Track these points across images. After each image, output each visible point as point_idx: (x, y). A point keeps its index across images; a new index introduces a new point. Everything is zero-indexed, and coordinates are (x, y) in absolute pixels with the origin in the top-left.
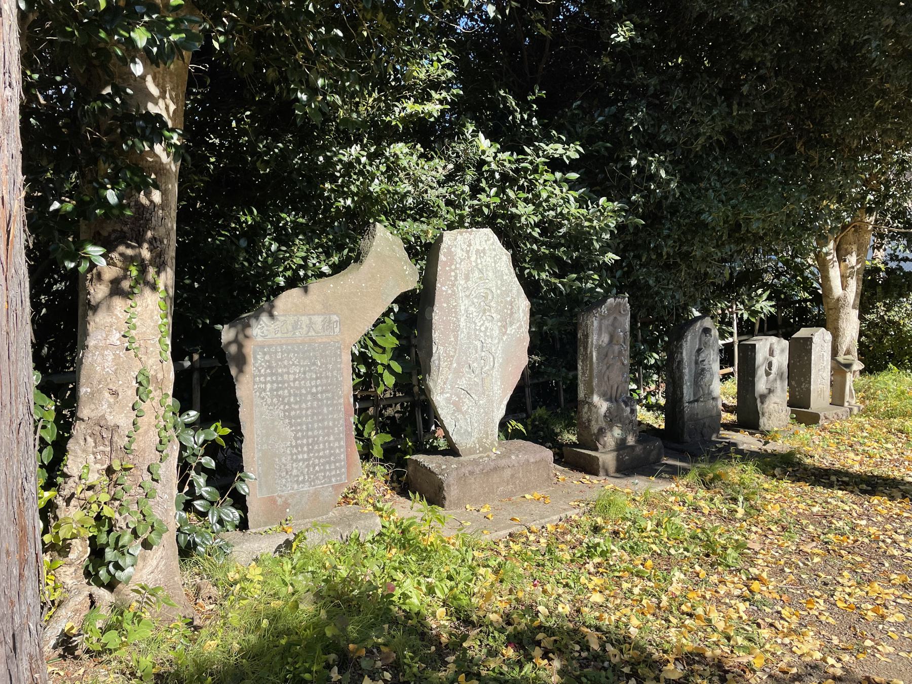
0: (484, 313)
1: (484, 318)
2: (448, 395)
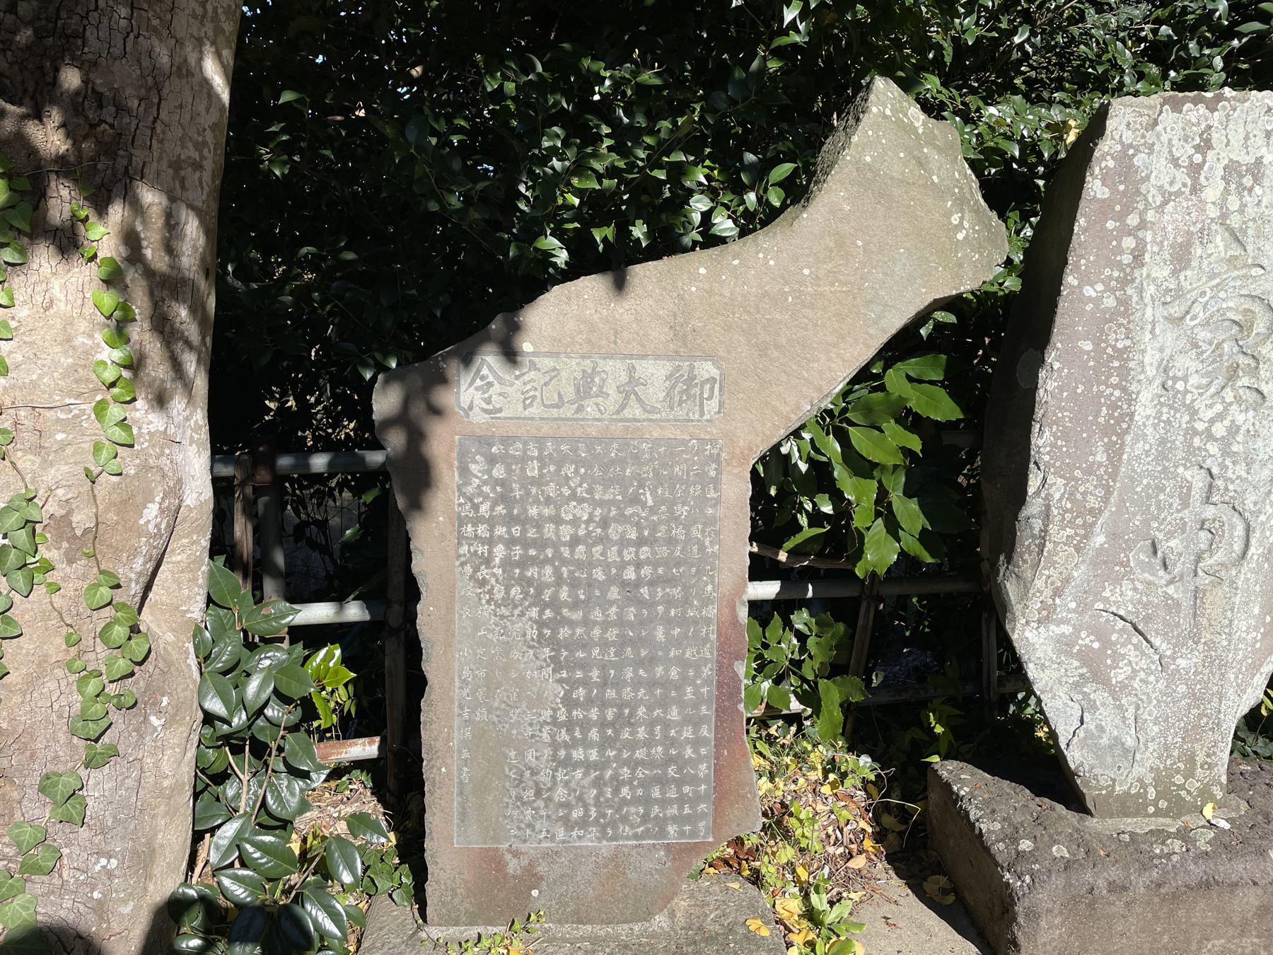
2: (1067, 629)
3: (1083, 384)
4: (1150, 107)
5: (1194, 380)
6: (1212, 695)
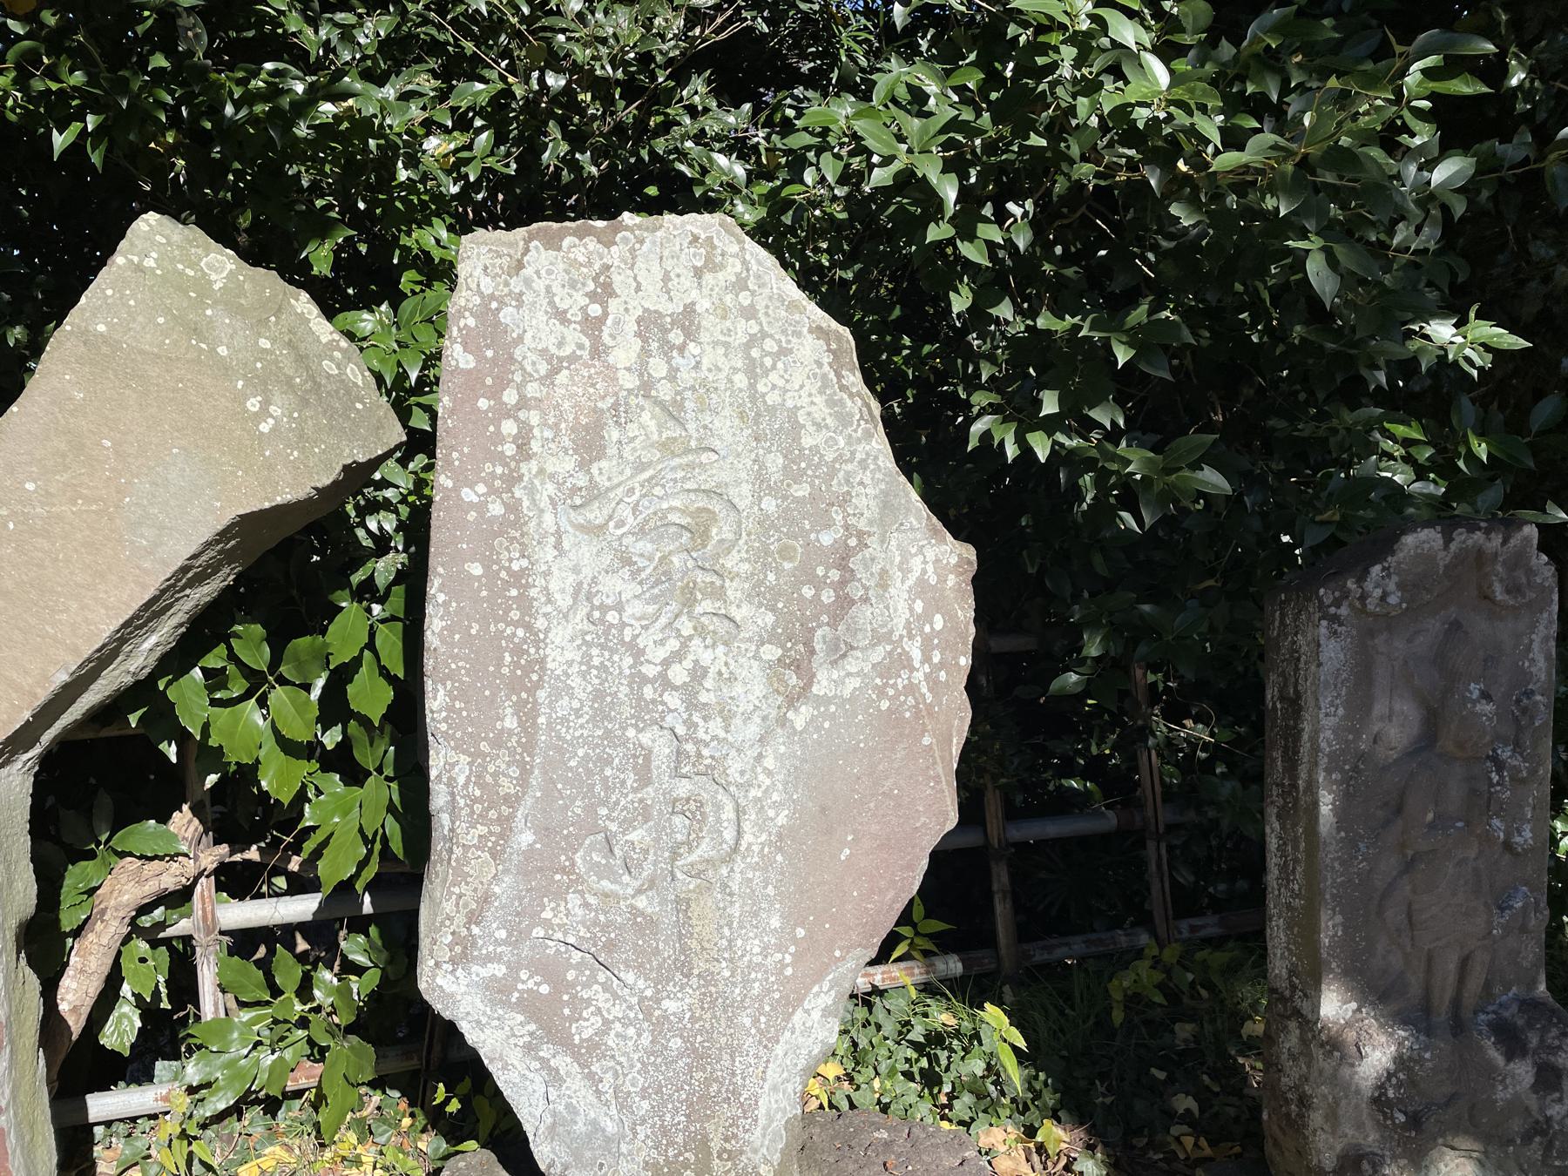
0: (689, 602)
1: (686, 627)
2: (499, 970)
3: (477, 621)
4: (510, 245)
5: (635, 609)
6: (720, 1049)
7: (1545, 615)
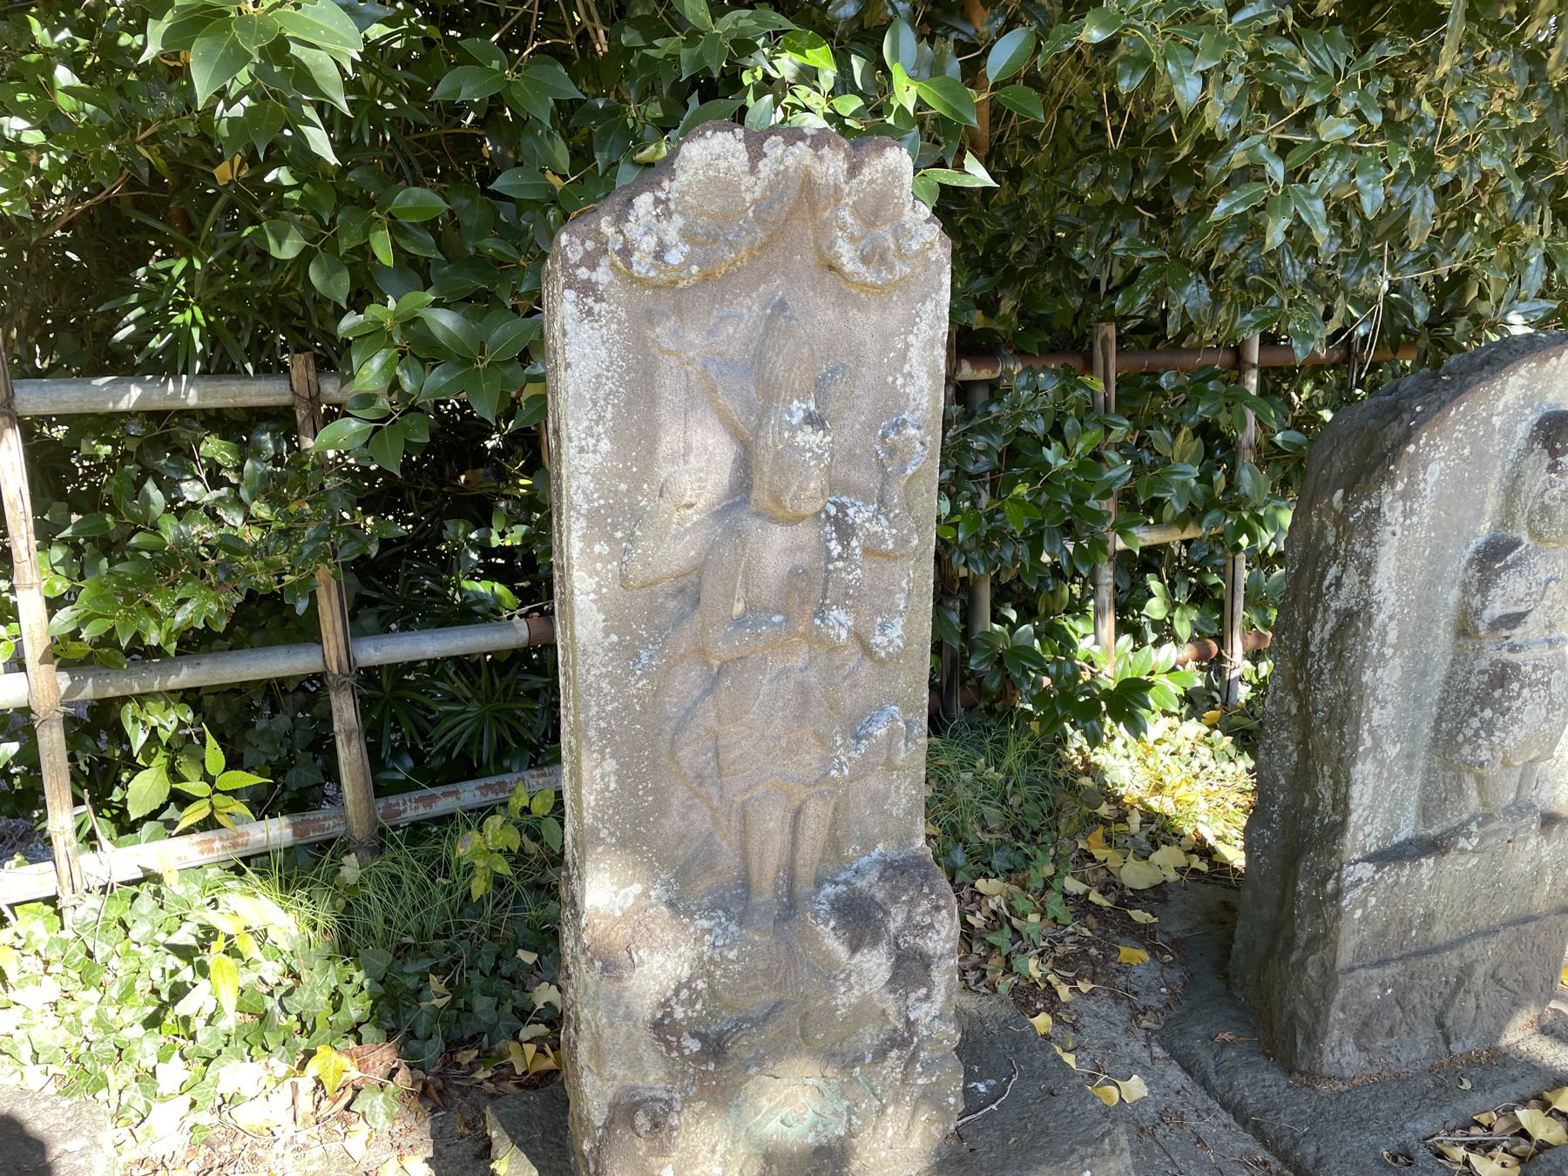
7: (929, 306)
